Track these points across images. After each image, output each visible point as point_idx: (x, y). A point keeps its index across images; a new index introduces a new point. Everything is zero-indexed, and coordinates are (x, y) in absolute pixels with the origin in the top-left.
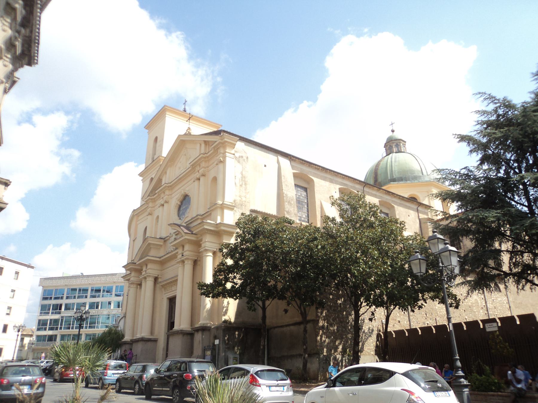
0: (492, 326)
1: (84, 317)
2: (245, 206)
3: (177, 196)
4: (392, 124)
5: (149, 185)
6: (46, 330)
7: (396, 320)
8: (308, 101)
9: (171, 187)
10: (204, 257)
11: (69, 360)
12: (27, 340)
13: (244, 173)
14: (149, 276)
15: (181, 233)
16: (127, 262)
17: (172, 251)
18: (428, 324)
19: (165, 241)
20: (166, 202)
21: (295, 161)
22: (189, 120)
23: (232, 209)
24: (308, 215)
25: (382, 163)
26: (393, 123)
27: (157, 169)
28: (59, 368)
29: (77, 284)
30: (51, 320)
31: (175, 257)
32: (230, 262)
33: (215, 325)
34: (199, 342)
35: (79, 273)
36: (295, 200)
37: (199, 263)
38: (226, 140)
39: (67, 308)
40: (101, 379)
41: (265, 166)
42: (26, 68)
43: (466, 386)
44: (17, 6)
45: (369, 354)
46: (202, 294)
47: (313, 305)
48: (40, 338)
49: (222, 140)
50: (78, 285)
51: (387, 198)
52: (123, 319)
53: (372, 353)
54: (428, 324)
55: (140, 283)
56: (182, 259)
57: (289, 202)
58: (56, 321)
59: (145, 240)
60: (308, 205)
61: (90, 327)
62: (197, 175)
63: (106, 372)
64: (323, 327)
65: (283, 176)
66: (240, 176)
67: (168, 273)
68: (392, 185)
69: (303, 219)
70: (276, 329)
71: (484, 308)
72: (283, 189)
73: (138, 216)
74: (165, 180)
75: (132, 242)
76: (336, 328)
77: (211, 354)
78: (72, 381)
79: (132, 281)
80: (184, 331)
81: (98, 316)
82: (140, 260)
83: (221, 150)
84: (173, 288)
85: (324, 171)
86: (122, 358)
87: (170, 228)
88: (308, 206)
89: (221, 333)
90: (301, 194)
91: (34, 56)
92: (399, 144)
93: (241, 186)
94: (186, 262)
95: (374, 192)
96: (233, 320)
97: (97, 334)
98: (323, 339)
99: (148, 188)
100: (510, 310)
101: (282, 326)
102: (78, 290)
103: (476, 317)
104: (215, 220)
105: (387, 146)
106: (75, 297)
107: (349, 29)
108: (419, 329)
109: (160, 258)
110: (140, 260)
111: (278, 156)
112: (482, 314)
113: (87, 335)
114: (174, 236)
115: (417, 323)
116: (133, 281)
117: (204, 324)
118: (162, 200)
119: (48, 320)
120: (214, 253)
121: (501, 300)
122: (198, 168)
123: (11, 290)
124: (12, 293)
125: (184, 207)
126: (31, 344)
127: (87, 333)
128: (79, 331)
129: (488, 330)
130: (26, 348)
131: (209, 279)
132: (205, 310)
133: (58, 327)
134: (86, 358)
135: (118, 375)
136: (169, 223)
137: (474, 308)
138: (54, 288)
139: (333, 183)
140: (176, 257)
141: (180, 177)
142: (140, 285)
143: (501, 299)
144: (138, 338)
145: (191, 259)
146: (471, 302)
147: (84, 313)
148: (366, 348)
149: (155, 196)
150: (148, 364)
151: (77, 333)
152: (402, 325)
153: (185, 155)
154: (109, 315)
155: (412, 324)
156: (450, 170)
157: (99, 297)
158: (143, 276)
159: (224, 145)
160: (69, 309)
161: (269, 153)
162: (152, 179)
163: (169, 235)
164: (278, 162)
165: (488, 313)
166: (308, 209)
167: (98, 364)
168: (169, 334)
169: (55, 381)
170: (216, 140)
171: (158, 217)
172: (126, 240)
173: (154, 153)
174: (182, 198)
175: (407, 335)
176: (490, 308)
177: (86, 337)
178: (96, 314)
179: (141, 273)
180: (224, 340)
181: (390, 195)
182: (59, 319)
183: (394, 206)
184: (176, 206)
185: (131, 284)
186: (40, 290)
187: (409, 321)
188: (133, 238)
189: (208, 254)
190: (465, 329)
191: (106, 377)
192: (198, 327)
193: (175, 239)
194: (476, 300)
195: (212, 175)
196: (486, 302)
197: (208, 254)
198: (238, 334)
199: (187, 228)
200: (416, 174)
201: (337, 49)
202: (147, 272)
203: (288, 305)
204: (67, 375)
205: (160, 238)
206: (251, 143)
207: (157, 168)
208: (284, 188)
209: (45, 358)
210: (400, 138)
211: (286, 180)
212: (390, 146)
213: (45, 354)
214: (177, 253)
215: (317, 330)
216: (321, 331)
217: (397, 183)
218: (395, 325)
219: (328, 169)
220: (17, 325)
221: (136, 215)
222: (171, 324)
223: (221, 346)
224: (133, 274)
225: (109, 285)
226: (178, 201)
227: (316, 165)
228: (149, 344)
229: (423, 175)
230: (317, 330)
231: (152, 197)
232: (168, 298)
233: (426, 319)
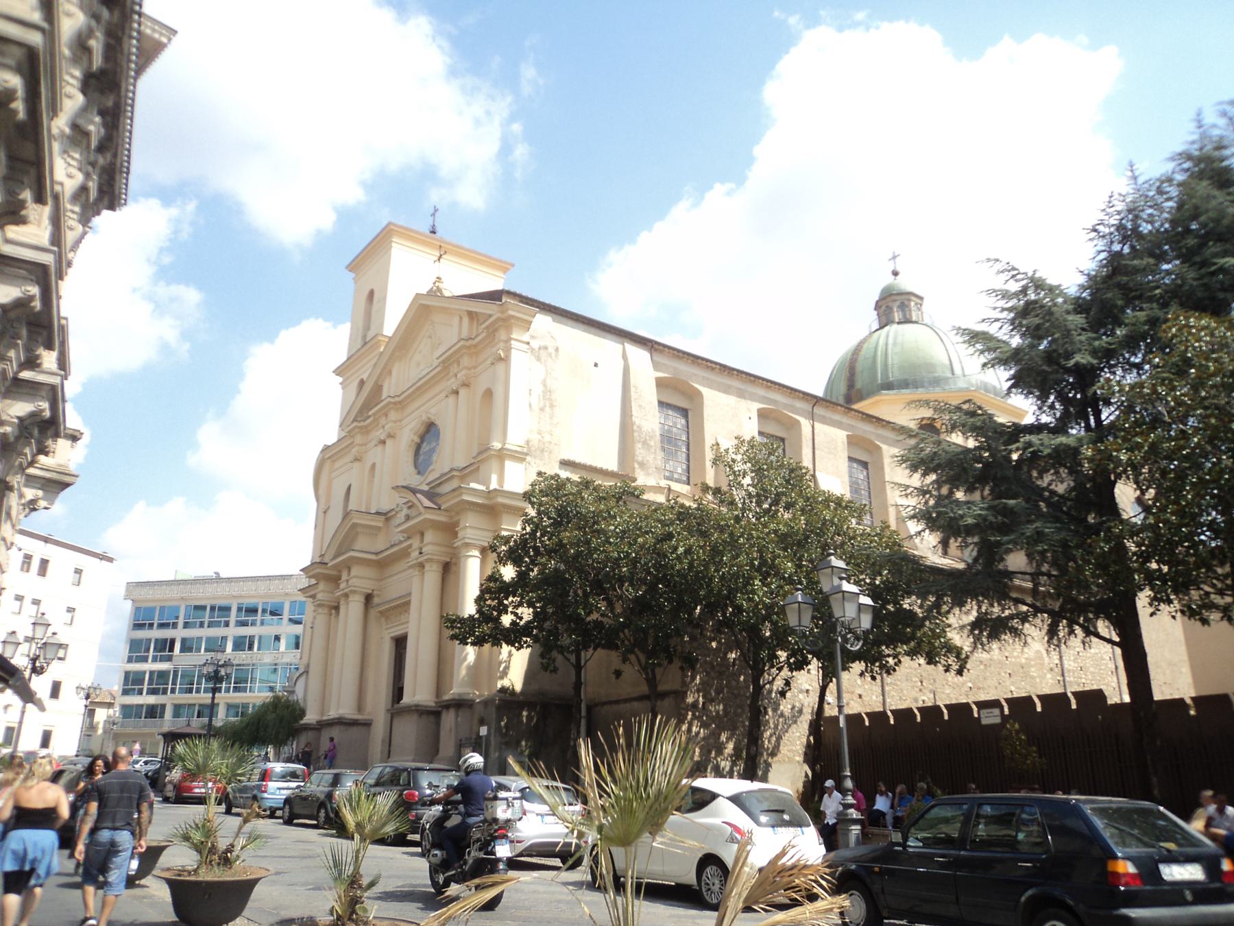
1: (223, 672)
2: (551, 452)
4: (894, 257)
6: (141, 694)
7: (853, 693)
8: (723, 182)
9: (401, 404)
10: (462, 560)
11: (197, 766)
12: (101, 715)
13: (548, 383)
14: (354, 592)
17: (401, 542)
18: (924, 701)
19: (387, 520)
20: (390, 436)
21: (661, 352)
23: (522, 460)
24: (688, 467)
25: (865, 346)
27: (373, 362)
28: (175, 774)
29: (206, 596)
30: (152, 673)
31: (405, 553)
32: (509, 573)
33: (483, 696)
35: (209, 572)
36: (658, 438)
37: (453, 568)
38: (511, 312)
39: (187, 647)
40: (255, 798)
41: (596, 365)
42: (106, 213)
43: (855, 822)
44: (92, 128)
45: (791, 760)
46: (453, 637)
47: (671, 662)
48: (127, 710)
49: (503, 312)
50: (209, 598)
51: (867, 429)
53: (798, 758)
54: (924, 701)
56: (419, 560)
57: (645, 443)
58: (163, 675)
59: (346, 514)
60: (688, 445)
61: (236, 689)
62: (452, 383)
63: (266, 785)
64: (694, 706)
66: (541, 388)
67: (393, 589)
68: (884, 398)
69: (676, 476)
70: (606, 708)
71: (1056, 670)
73: (334, 461)
74: (390, 388)
75: (321, 515)
76: (721, 707)
78: (201, 800)
80: (422, 706)
81: (253, 665)
82: (335, 557)
83: (502, 335)
86: (297, 760)
87: (395, 495)
88: (688, 450)
89: (492, 711)
90: (675, 423)
91: (120, 193)
92: (906, 302)
93: (542, 409)
94: (427, 567)
95: (837, 417)
96: (518, 687)
98: (694, 729)
100: (1117, 675)
101: (617, 702)
102: (208, 609)
104: (486, 482)
106: (202, 625)
107: (822, 13)
108: (916, 711)
109: (377, 554)
110: (335, 557)
111: (626, 345)
112: (1051, 681)
113: (229, 706)
114: (405, 511)
115: (901, 699)
117: (460, 694)
118: (381, 431)
119: (144, 673)
120: (483, 551)
122: (454, 369)
123: (65, 609)
124: (70, 615)
125: (427, 448)
126: (110, 722)
127: (229, 701)
128: (213, 698)
129: (984, 722)
130: (100, 731)
131: (469, 609)
132: (466, 664)
134: (222, 764)
135: (289, 792)
136: (394, 485)
137: (1033, 669)
138: (158, 605)
139: (745, 398)
140: (408, 555)
141: (418, 384)
142: (337, 608)
143: (1097, 651)
145: (438, 562)
146: (1026, 656)
148: (784, 749)
150: (344, 771)
151: (209, 701)
153: (430, 337)
154: (276, 664)
155: (888, 700)
157: (253, 624)
159: (506, 323)
160: (190, 650)
161: (604, 338)
162: (362, 383)
163: (394, 506)
164: (624, 356)
165: (1064, 681)
166: (688, 455)
167: (240, 772)
169: (166, 800)
170: (490, 312)
171: (373, 466)
172: (310, 506)
173: (367, 327)
174: (422, 429)
175: (867, 723)
176: (1069, 671)
177: (228, 710)
178: (249, 661)
179: (338, 585)
180: (499, 728)
181: (871, 422)
183: (881, 445)
184: (410, 446)
185: (319, 606)
186: (128, 606)
187: (883, 695)
188: (323, 507)
189: (470, 553)
190: (946, 717)
191: (266, 795)
193: (408, 518)
194: (1038, 652)
195: (481, 385)
196: (1061, 658)
197: (470, 553)
198: (527, 717)
199: (431, 495)
200: (939, 373)
201: (788, 65)
202: (350, 583)
203: (625, 660)
204: (190, 789)
205: (378, 513)
208: (634, 413)
209: (142, 753)
210: (909, 289)
213: (141, 745)
214: (410, 546)
215: (683, 712)
216: (690, 713)
217: (895, 391)
218: (852, 702)
219: (734, 369)
220: (84, 686)
221: (329, 458)
222: (398, 692)
223: (492, 739)
224: (321, 586)
225: (276, 600)
226: (415, 434)
227: (707, 360)
228: (355, 730)
229: (953, 374)
230: (683, 712)
232: (392, 638)
233: (921, 690)
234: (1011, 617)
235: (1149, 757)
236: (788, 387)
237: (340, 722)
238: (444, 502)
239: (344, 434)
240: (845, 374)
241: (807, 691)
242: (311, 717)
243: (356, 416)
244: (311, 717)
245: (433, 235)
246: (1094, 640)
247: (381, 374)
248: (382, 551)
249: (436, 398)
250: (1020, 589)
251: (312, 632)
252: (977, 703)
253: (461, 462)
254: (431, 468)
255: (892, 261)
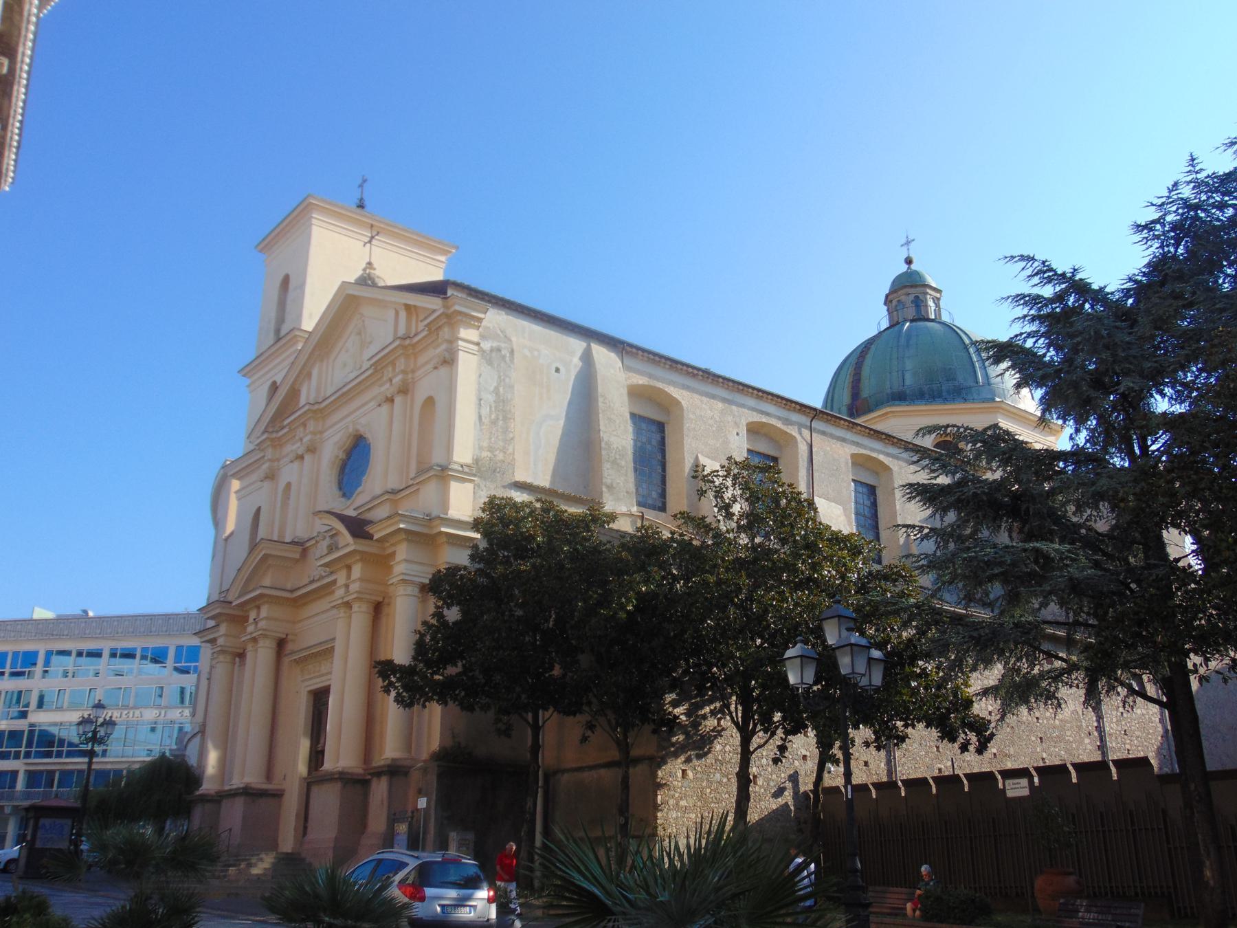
0: (1017, 786)
3: (336, 438)
4: (908, 243)
5: (267, 405)
9: (321, 411)
15: (343, 534)
16: (208, 599)
17: (322, 578)
18: (940, 770)
21: (634, 355)
22: (370, 242)
26: (911, 238)
27: (292, 359)
34: (382, 801)
38: (457, 308)
52: (199, 736)
54: (940, 770)
55: (241, 651)
57: (614, 462)
59: (253, 546)
62: (386, 389)
65: (603, 396)
72: (599, 430)
77: (409, 832)
79: (221, 646)
80: (348, 773)
83: (445, 333)
84: (324, 670)
85: (710, 380)
92: (921, 297)
94: (356, 607)
97: (125, 772)
99: (264, 411)
103: (1071, 755)
105: (891, 301)
109: (292, 591)
110: (239, 597)
112: (1089, 747)
116: (225, 646)
117: (344, 768)
118: (388, 385)
121: (1143, 715)
129: (1010, 794)
133: (26, 747)
141: (345, 390)
142: (242, 655)
144: (234, 787)
147: (102, 725)
149: (281, 433)
151: (85, 767)
152: (874, 772)
156: (963, 427)
158: (249, 637)
159: (452, 319)
162: (274, 387)
168: (309, 780)
170: (434, 307)
171: (289, 485)
173: (281, 319)
179: (245, 628)
181: (881, 440)
182: (24, 731)
185: (223, 652)
192: (379, 767)
195: (420, 395)
205: (293, 543)
206: (522, 313)
207: (288, 357)
208: (602, 428)
211: (610, 406)
212: (899, 301)
214: (335, 582)
219: (719, 377)
222: (317, 756)
224: (223, 629)
227: (688, 366)
231: (274, 435)
232: (310, 692)
234: (1042, 675)
235: (1200, 836)
236: (782, 398)
237: (248, 793)
238: (377, 531)
239: (252, 447)
240: (847, 380)
241: (804, 757)
242: (208, 787)
243: (267, 426)
244: (208, 787)
245: (359, 210)
246: (1139, 700)
247: (298, 376)
248: (299, 588)
249: (366, 408)
250: (1054, 639)
251: (209, 684)
252: (1002, 772)
253: (393, 482)
254: (360, 489)
255: (905, 248)
